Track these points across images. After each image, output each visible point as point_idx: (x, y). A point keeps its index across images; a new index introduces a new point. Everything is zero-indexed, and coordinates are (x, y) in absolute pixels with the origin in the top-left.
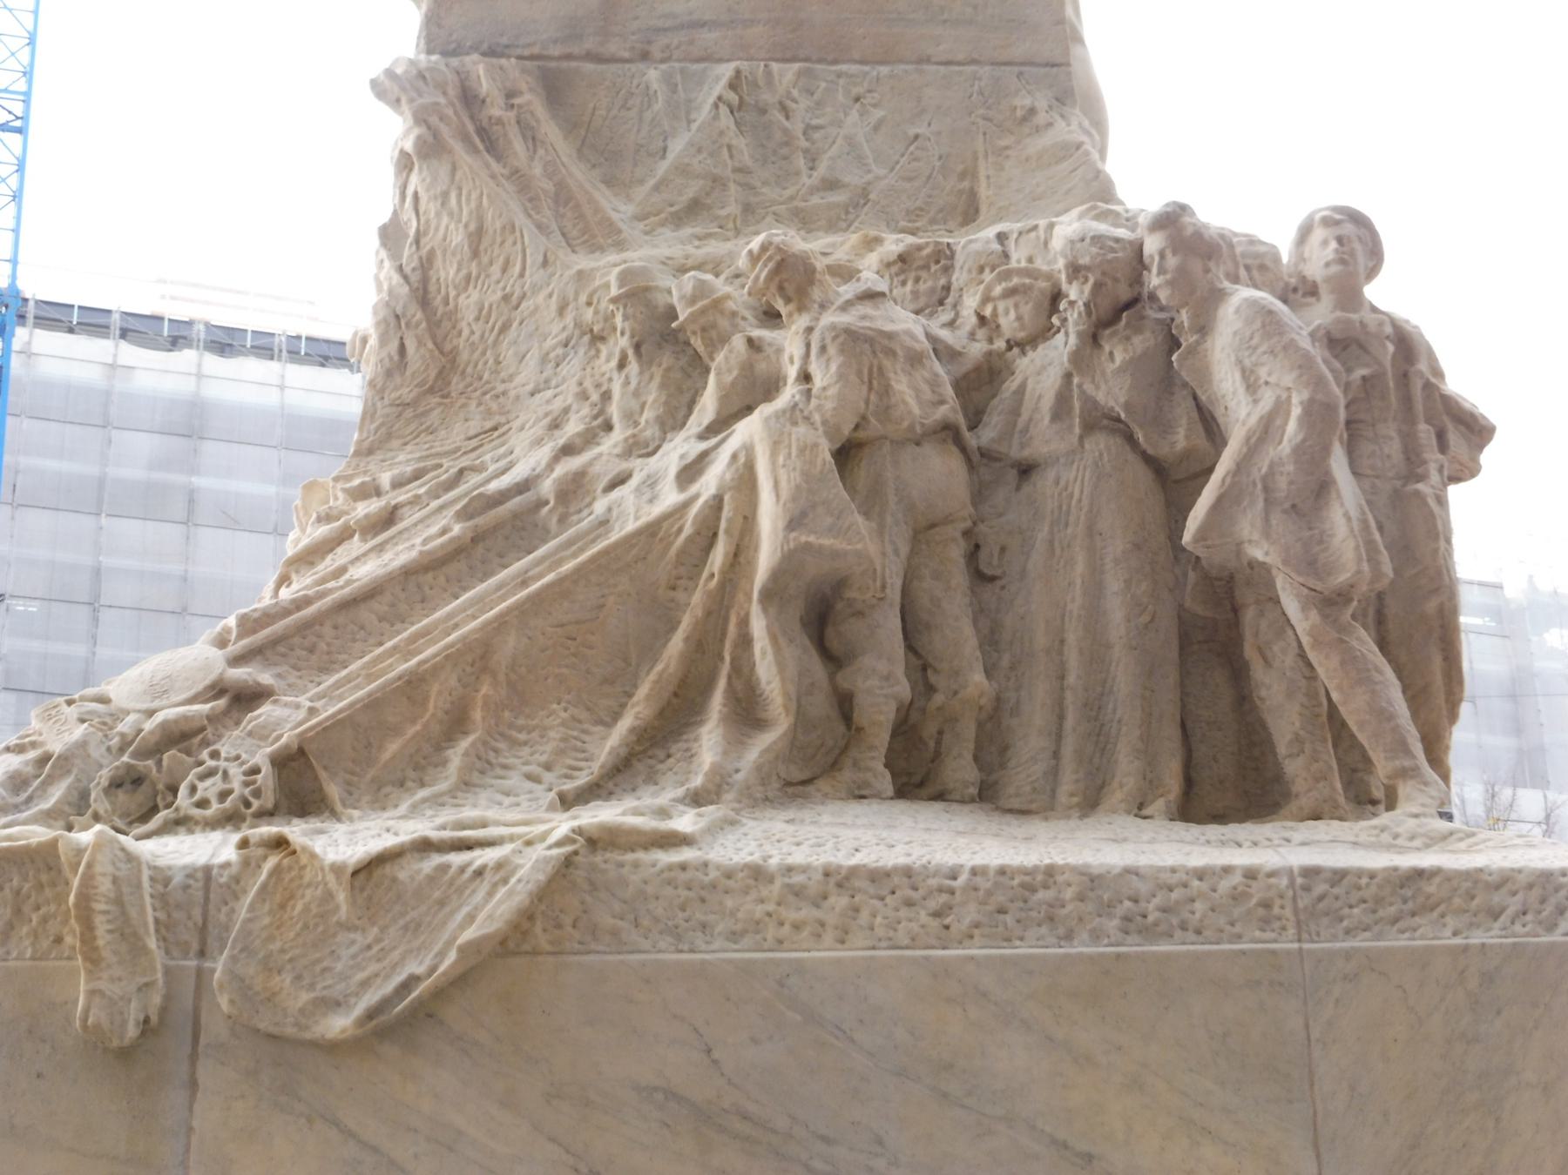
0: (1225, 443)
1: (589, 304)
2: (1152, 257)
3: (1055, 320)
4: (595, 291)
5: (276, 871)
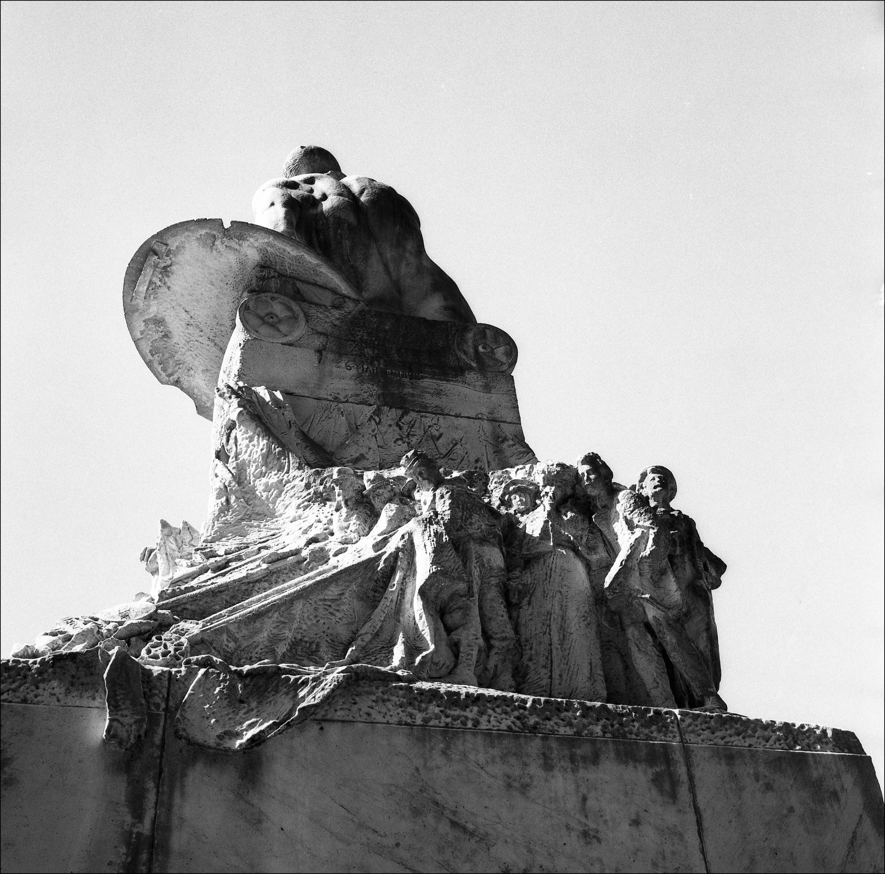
0: (619, 550)
1: (321, 484)
2: (583, 474)
3: (538, 502)
4: (325, 478)
5: (206, 674)
